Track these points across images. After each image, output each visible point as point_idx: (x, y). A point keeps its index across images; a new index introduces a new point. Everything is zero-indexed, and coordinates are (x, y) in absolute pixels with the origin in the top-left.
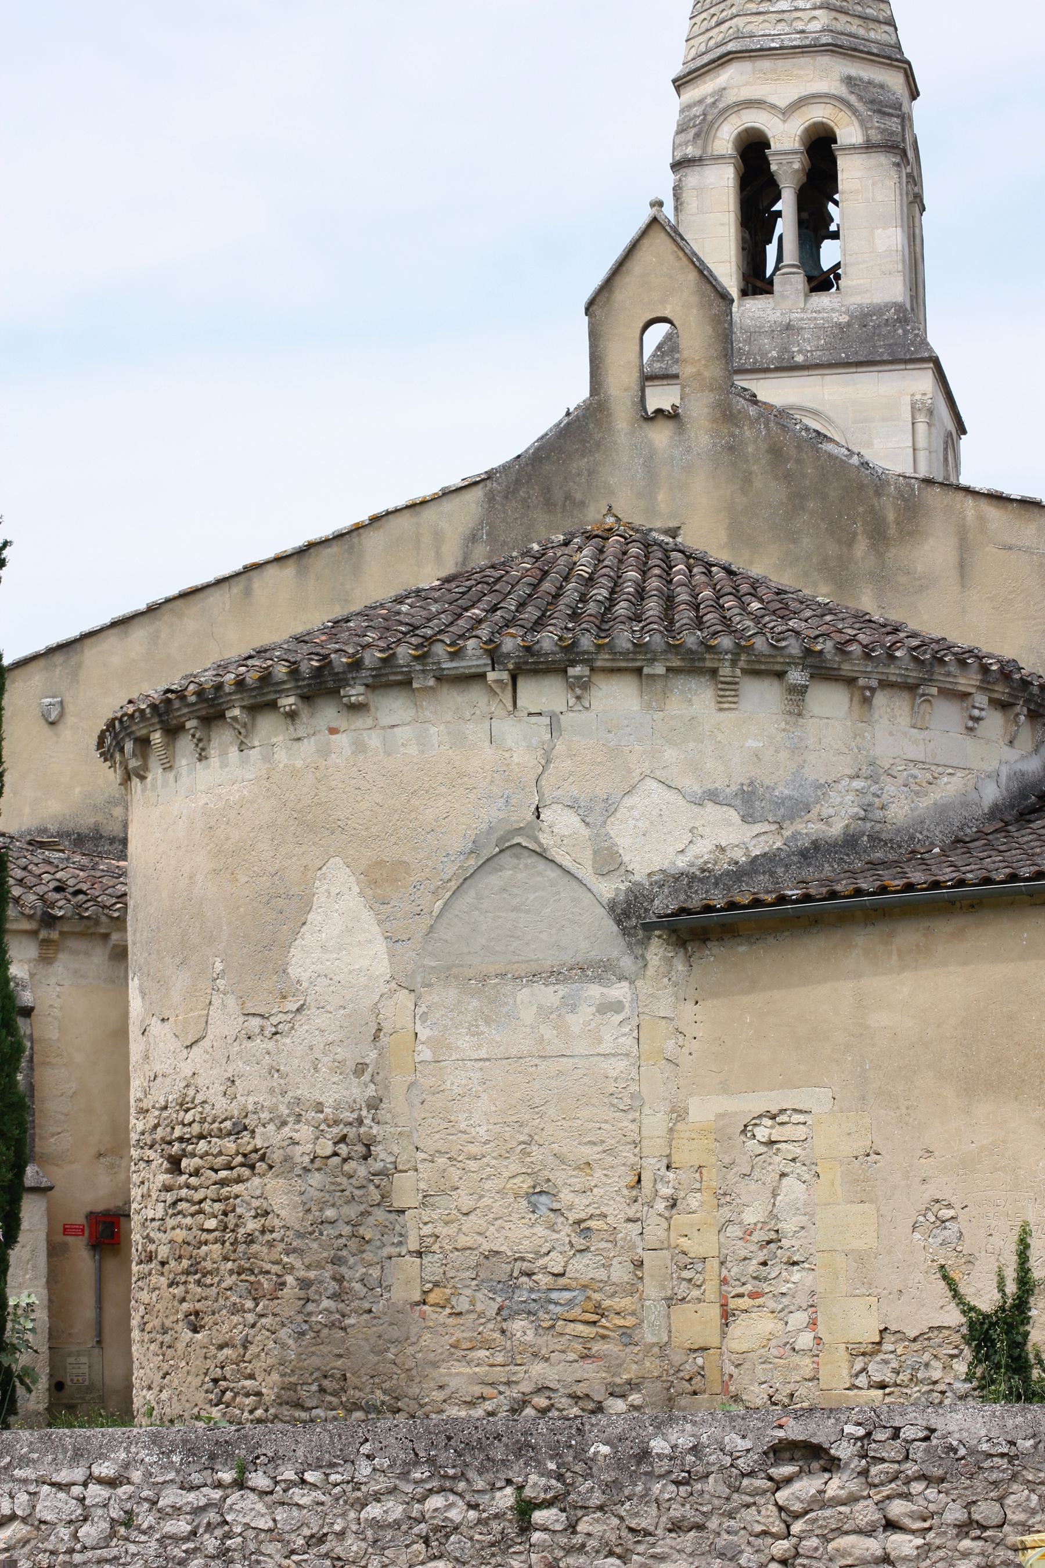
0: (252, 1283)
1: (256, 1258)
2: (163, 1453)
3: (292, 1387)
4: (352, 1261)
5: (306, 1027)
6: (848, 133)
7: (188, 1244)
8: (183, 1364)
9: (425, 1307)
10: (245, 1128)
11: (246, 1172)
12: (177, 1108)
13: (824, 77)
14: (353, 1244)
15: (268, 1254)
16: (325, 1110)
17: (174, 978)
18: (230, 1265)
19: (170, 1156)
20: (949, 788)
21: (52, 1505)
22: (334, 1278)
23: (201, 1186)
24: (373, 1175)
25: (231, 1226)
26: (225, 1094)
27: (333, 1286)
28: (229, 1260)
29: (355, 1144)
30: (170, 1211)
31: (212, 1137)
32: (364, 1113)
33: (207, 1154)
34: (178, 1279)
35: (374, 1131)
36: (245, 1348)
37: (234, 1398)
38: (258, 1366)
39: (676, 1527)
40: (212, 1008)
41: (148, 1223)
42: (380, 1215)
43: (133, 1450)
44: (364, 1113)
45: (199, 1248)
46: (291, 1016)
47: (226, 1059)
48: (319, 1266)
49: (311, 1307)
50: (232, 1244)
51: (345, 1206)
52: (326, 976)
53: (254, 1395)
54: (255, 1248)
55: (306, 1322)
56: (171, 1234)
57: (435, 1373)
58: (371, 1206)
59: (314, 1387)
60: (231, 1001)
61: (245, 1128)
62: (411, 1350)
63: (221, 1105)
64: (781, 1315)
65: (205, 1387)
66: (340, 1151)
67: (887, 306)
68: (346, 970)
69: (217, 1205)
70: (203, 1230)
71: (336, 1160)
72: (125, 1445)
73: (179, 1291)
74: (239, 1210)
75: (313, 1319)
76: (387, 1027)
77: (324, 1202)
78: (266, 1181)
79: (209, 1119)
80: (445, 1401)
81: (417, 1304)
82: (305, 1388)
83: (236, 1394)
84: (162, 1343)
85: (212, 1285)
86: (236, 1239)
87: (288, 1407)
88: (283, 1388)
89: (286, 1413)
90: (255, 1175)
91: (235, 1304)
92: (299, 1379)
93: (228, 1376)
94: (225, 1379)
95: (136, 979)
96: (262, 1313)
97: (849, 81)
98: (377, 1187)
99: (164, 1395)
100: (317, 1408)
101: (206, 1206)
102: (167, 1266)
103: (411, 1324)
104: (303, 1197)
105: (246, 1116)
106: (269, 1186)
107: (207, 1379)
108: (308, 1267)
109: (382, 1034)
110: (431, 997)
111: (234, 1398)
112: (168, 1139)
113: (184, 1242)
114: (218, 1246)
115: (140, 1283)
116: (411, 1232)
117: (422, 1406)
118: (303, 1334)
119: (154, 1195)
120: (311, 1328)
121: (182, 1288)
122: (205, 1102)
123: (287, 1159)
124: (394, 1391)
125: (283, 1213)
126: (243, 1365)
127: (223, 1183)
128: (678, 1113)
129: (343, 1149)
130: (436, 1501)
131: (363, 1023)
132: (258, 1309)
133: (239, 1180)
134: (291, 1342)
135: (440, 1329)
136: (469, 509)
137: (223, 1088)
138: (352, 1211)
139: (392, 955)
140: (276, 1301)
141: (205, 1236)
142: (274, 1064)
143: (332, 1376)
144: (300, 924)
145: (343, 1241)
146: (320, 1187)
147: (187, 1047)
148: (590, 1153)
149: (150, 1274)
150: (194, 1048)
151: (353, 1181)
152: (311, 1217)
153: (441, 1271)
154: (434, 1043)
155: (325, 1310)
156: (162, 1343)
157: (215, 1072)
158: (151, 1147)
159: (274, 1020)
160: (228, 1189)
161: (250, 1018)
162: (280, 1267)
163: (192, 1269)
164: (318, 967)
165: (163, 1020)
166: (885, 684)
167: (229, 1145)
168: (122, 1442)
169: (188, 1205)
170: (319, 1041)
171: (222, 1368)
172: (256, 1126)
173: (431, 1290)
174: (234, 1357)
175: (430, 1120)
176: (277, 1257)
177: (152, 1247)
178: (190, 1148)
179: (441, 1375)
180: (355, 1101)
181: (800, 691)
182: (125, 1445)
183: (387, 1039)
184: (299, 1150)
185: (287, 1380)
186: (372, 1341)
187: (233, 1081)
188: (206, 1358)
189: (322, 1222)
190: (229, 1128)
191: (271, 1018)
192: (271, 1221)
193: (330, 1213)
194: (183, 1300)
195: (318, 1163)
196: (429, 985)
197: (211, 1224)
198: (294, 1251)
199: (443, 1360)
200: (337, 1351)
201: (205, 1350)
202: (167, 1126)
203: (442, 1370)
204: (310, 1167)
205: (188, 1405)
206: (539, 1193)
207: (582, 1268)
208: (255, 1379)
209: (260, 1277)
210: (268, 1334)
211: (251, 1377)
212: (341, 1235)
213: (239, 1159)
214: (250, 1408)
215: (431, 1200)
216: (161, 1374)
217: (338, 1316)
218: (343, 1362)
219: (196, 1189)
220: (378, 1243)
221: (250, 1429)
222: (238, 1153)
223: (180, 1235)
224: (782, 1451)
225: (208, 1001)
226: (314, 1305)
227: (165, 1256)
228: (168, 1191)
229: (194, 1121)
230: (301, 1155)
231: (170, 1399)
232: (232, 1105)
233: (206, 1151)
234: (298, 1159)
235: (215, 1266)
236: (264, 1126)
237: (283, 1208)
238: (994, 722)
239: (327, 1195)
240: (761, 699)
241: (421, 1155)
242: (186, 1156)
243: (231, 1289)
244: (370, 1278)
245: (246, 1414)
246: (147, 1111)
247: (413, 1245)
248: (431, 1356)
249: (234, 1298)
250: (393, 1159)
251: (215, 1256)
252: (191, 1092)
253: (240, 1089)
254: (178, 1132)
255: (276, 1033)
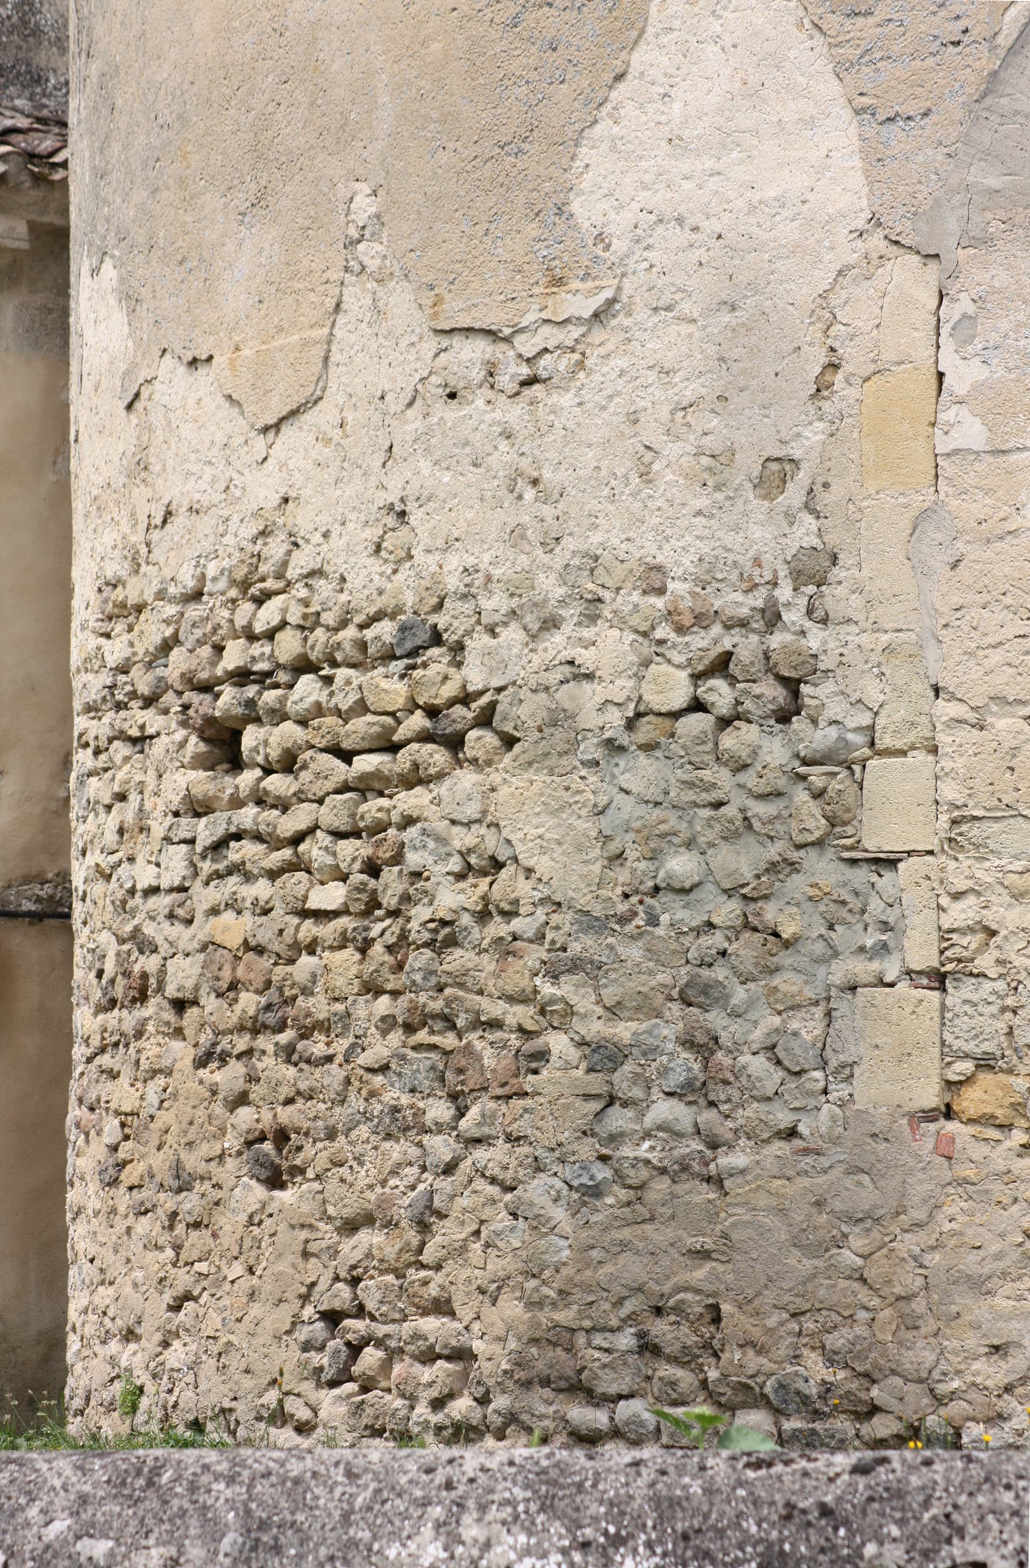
0: (447, 1053)
1: (461, 986)
2: (585, 1546)
3: (561, 1338)
4: (740, 995)
5: (619, 362)
7: (260, 950)
8: (237, 1269)
9: (952, 1127)
10: (436, 638)
11: (436, 756)
12: (233, 593)
14: (746, 950)
15: (497, 975)
16: (671, 586)
17: (230, 247)
18: (383, 1005)
19: (210, 721)
22: (688, 1043)
23: (300, 797)
24: (805, 762)
25: (389, 900)
26: (378, 548)
27: (685, 1065)
28: (379, 992)
29: (754, 678)
30: (207, 867)
31: (334, 664)
32: (784, 593)
33: (319, 710)
34: (224, 1044)
35: (814, 641)
36: (424, 1227)
37: (387, 1365)
38: (459, 1279)
40: (341, 319)
41: (138, 898)
42: (824, 870)
43: (471, 1530)
44: (784, 593)
45: (292, 961)
46: (576, 332)
47: (381, 456)
48: (645, 1007)
49: (619, 1119)
50: (390, 949)
51: (724, 848)
52: (680, 220)
53: (449, 1358)
54: (458, 958)
55: (604, 1159)
56: (203, 929)
57: (979, 1309)
58: (799, 847)
59: (626, 1340)
60: (401, 301)
61: (436, 638)
62: (909, 1243)
63: (366, 581)
65: (303, 1334)
66: (709, 698)
68: (740, 203)
69: (347, 848)
70: (305, 914)
71: (697, 723)
72: (437, 1512)
73: (228, 1077)
74: (413, 859)
75: (627, 1151)
76: (855, 359)
77: (662, 836)
78: (496, 778)
79: (329, 618)
80: (1008, 1389)
81: (929, 1116)
82: (598, 1340)
83: (393, 1355)
84: (174, 1215)
85: (329, 1059)
86: (404, 935)
87: (547, 1393)
88: (534, 1341)
89: (542, 1409)
90: (459, 763)
91: (396, 1110)
92: (581, 1315)
93: (371, 1305)
94: (360, 1311)
95: (108, 270)
96: (476, 1133)
98: (818, 795)
99: (177, 1355)
100: (630, 1396)
101: (313, 850)
102: (192, 1013)
103: (910, 1172)
104: (604, 822)
105: (440, 606)
106: (504, 791)
107: (309, 1311)
108: (614, 1011)
109: (839, 377)
110: (984, 274)
111: (387, 1365)
112: (204, 675)
113: (247, 946)
114: (349, 954)
115: (105, 1060)
116: (913, 920)
117: (939, 1400)
118: (595, 1191)
119: (158, 829)
120: (619, 1175)
121: (236, 1069)
122: (317, 573)
123: (557, 719)
124: (861, 1356)
125: (543, 865)
126: (414, 1275)
127: (365, 787)
129: (720, 693)
131: (786, 347)
132: (463, 1124)
133: (415, 778)
134: (559, 1214)
135: (997, 1188)
137: (373, 533)
138: (742, 861)
139: (875, 160)
140: (518, 1103)
141: (309, 929)
142: (524, 463)
143: (678, 1309)
144: (609, 77)
145: (717, 940)
146: (653, 793)
147: (266, 430)
149: (139, 1034)
150: (286, 429)
151: (749, 778)
152: (623, 875)
153: (1002, 1026)
155: (660, 1128)
156: (174, 1215)
157: (349, 491)
158: (149, 702)
159: (527, 345)
160: (384, 802)
161: (457, 341)
162: (531, 1010)
163: (271, 1019)
164: (659, 199)
165: (194, 362)
167: (388, 686)
168: (425, 1503)
169: (261, 848)
170: (657, 400)
171: (355, 1282)
172: (469, 633)
173: (968, 1080)
174: (390, 1252)
175: (975, 613)
176: (524, 983)
177: (150, 963)
178: (270, 697)
179: (999, 1316)
180: (757, 562)
182: (437, 1512)
183: (853, 392)
184: (591, 694)
185: (546, 1316)
186: (798, 1218)
187: (403, 514)
188: (306, 1255)
189: (657, 889)
190: (388, 639)
191: (518, 340)
192: (509, 884)
193: (680, 865)
194: (242, 1099)
195: (646, 730)
196: (984, 241)
197: (329, 896)
198: (575, 966)
199: (1004, 1275)
200: (694, 1242)
201: (304, 1234)
202: (200, 643)
203: (1001, 1303)
204: (624, 739)
205: (248, 1383)
208: (452, 1314)
209: (473, 1037)
210: (494, 1190)
211: (442, 1307)
212: (710, 925)
213: (418, 721)
214: (434, 1393)
215: (974, 831)
216: (168, 1298)
217: (697, 1145)
218: (712, 1272)
219: (284, 806)
220: (819, 948)
221: (911, 1468)
222: (413, 706)
223: (232, 929)
225: (330, 303)
226: (629, 1113)
227: (189, 984)
228: (198, 815)
229: (283, 624)
230: (596, 708)
231: (194, 1366)
232: (400, 577)
233: (318, 704)
234: (589, 719)
235: (339, 1007)
236: (492, 631)
237: (543, 851)
239: (672, 817)
241: (946, 709)
242: (258, 720)
243: (384, 1069)
244: (795, 1044)
245: (422, 1410)
246: (139, 609)
247: (921, 952)
248: (970, 1262)
249: (394, 1095)
250: (866, 719)
251: (340, 982)
252: (276, 548)
253: (424, 538)
254: (234, 656)
255: (529, 382)
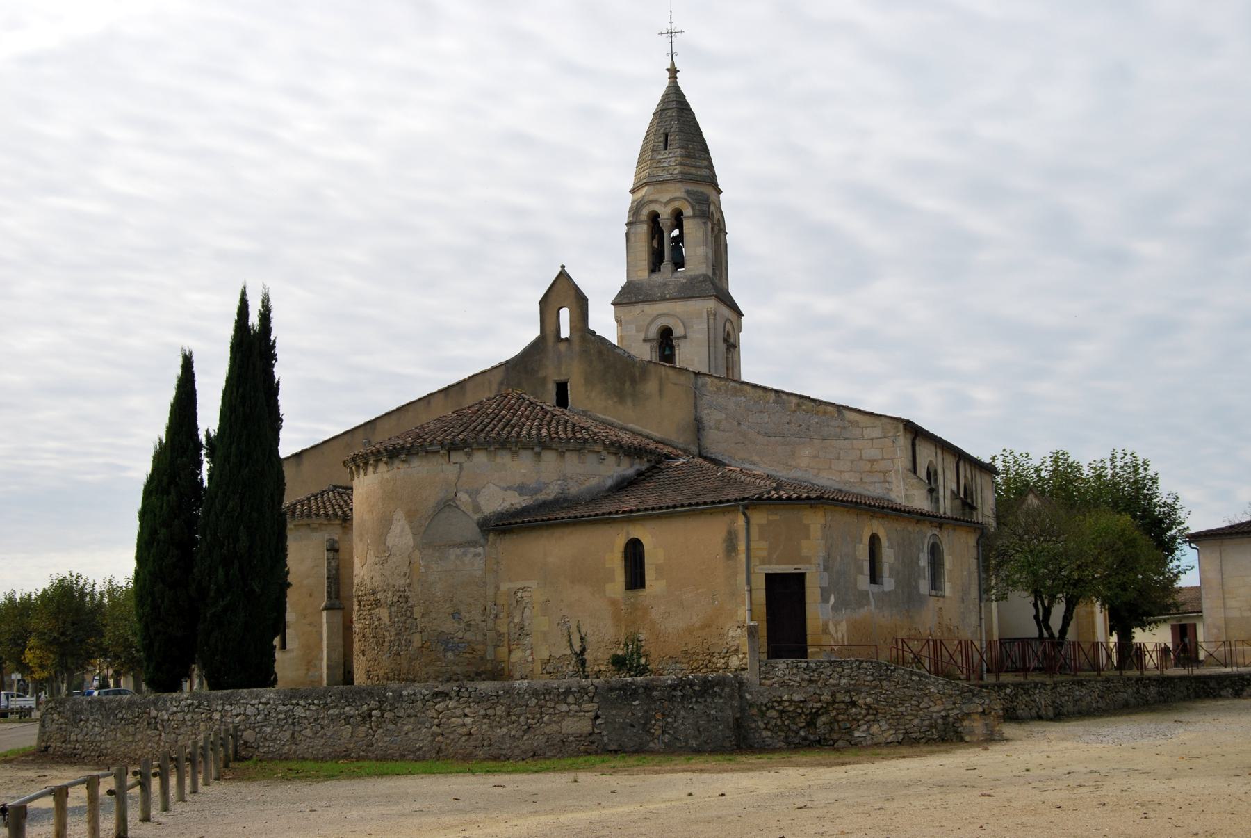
6: (688, 212)
13: (678, 191)
20: (593, 482)
21: (250, 710)
39: (409, 716)
64: (524, 651)
67: (699, 276)
97: (688, 192)
128: (498, 588)
130: (347, 709)
136: (499, 376)
148: (471, 600)
154: (425, 567)
166: (568, 450)
181: (539, 454)
206: (456, 615)
207: (469, 636)
224: (436, 694)
238: (611, 460)
240: (526, 456)
